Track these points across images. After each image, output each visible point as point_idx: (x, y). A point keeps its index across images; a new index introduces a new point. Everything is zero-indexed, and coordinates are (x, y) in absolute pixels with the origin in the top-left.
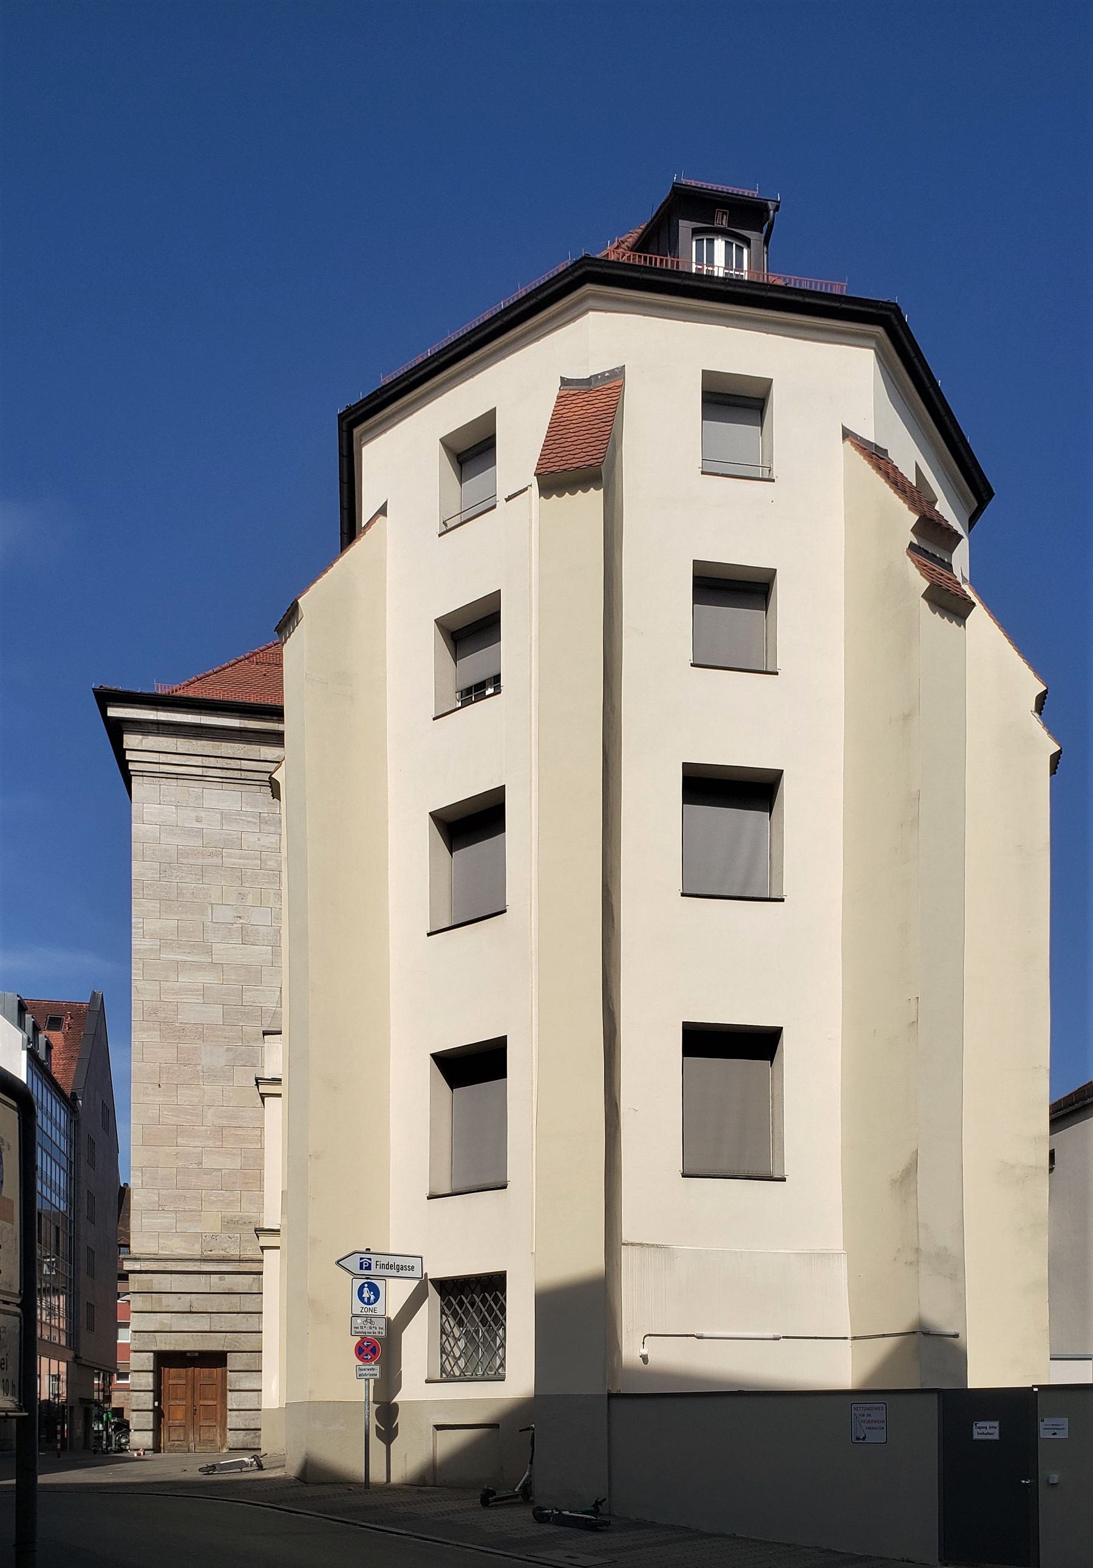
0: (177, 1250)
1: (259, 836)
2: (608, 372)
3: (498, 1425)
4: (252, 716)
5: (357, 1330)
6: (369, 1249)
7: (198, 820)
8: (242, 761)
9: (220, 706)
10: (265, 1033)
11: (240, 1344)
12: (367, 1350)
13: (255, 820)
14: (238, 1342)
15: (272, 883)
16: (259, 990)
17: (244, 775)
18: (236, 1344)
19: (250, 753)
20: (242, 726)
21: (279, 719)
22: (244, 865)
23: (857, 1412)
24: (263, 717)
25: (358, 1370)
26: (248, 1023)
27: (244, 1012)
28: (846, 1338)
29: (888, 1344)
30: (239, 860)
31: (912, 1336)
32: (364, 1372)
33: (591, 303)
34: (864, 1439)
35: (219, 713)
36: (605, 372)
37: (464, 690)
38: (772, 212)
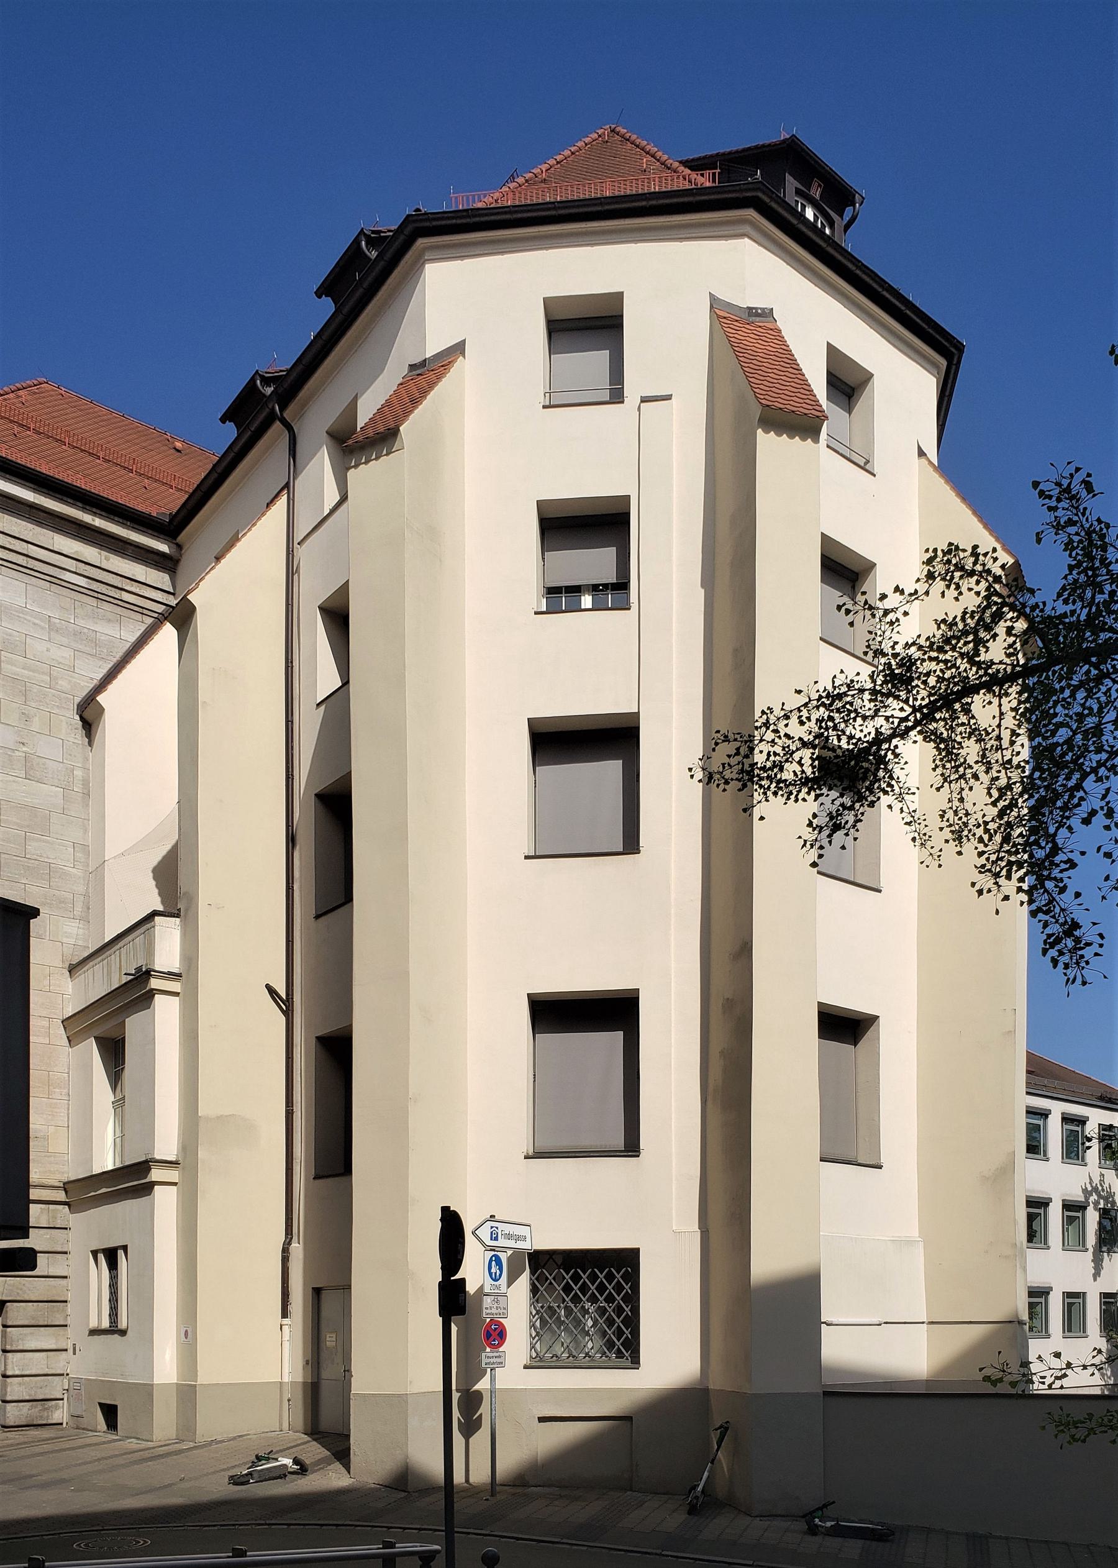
1: (49, 646)
2: (760, 308)
3: (632, 1417)
4: (51, 493)
6: (494, 1216)
8: (29, 545)
9: (13, 468)
11: (25, 1292)
12: (495, 1335)
13: (43, 624)
14: (21, 1289)
15: (64, 708)
16: (44, 841)
17: (32, 563)
18: (19, 1291)
19: (42, 538)
20: (36, 502)
21: (85, 506)
22: (28, 678)
24: (65, 498)
26: (32, 882)
27: (28, 867)
28: (923, 1323)
29: (975, 1333)
30: (23, 671)
31: (1010, 1325)
32: (492, 1360)
33: (747, 229)
35: (8, 476)
38: (857, 205)
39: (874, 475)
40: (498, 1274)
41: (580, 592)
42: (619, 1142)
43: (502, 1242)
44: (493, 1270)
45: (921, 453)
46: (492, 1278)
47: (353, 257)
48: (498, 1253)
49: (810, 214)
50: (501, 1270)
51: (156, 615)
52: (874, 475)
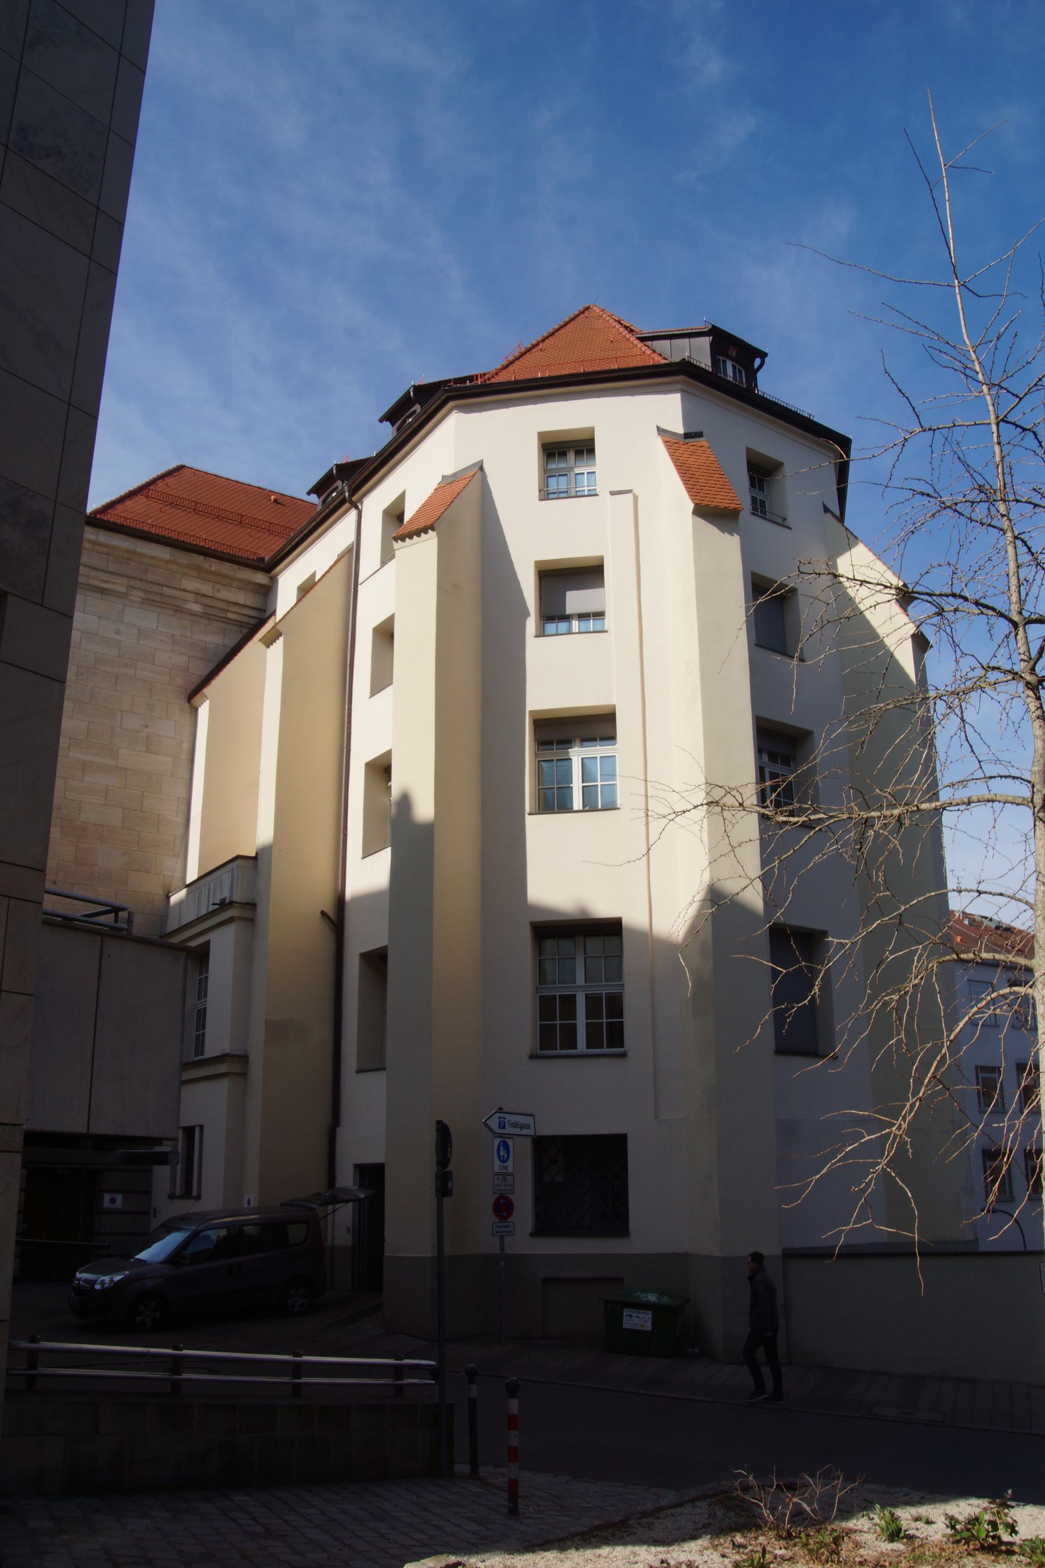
0: (940, 782)
5: (498, 1188)
7: (118, 632)
36: (692, 433)
37: (576, 614)
39: (790, 529)
43: (509, 1130)
44: (502, 1153)
45: (826, 510)
46: (500, 1160)
48: (506, 1140)
51: (251, 626)
52: (790, 529)
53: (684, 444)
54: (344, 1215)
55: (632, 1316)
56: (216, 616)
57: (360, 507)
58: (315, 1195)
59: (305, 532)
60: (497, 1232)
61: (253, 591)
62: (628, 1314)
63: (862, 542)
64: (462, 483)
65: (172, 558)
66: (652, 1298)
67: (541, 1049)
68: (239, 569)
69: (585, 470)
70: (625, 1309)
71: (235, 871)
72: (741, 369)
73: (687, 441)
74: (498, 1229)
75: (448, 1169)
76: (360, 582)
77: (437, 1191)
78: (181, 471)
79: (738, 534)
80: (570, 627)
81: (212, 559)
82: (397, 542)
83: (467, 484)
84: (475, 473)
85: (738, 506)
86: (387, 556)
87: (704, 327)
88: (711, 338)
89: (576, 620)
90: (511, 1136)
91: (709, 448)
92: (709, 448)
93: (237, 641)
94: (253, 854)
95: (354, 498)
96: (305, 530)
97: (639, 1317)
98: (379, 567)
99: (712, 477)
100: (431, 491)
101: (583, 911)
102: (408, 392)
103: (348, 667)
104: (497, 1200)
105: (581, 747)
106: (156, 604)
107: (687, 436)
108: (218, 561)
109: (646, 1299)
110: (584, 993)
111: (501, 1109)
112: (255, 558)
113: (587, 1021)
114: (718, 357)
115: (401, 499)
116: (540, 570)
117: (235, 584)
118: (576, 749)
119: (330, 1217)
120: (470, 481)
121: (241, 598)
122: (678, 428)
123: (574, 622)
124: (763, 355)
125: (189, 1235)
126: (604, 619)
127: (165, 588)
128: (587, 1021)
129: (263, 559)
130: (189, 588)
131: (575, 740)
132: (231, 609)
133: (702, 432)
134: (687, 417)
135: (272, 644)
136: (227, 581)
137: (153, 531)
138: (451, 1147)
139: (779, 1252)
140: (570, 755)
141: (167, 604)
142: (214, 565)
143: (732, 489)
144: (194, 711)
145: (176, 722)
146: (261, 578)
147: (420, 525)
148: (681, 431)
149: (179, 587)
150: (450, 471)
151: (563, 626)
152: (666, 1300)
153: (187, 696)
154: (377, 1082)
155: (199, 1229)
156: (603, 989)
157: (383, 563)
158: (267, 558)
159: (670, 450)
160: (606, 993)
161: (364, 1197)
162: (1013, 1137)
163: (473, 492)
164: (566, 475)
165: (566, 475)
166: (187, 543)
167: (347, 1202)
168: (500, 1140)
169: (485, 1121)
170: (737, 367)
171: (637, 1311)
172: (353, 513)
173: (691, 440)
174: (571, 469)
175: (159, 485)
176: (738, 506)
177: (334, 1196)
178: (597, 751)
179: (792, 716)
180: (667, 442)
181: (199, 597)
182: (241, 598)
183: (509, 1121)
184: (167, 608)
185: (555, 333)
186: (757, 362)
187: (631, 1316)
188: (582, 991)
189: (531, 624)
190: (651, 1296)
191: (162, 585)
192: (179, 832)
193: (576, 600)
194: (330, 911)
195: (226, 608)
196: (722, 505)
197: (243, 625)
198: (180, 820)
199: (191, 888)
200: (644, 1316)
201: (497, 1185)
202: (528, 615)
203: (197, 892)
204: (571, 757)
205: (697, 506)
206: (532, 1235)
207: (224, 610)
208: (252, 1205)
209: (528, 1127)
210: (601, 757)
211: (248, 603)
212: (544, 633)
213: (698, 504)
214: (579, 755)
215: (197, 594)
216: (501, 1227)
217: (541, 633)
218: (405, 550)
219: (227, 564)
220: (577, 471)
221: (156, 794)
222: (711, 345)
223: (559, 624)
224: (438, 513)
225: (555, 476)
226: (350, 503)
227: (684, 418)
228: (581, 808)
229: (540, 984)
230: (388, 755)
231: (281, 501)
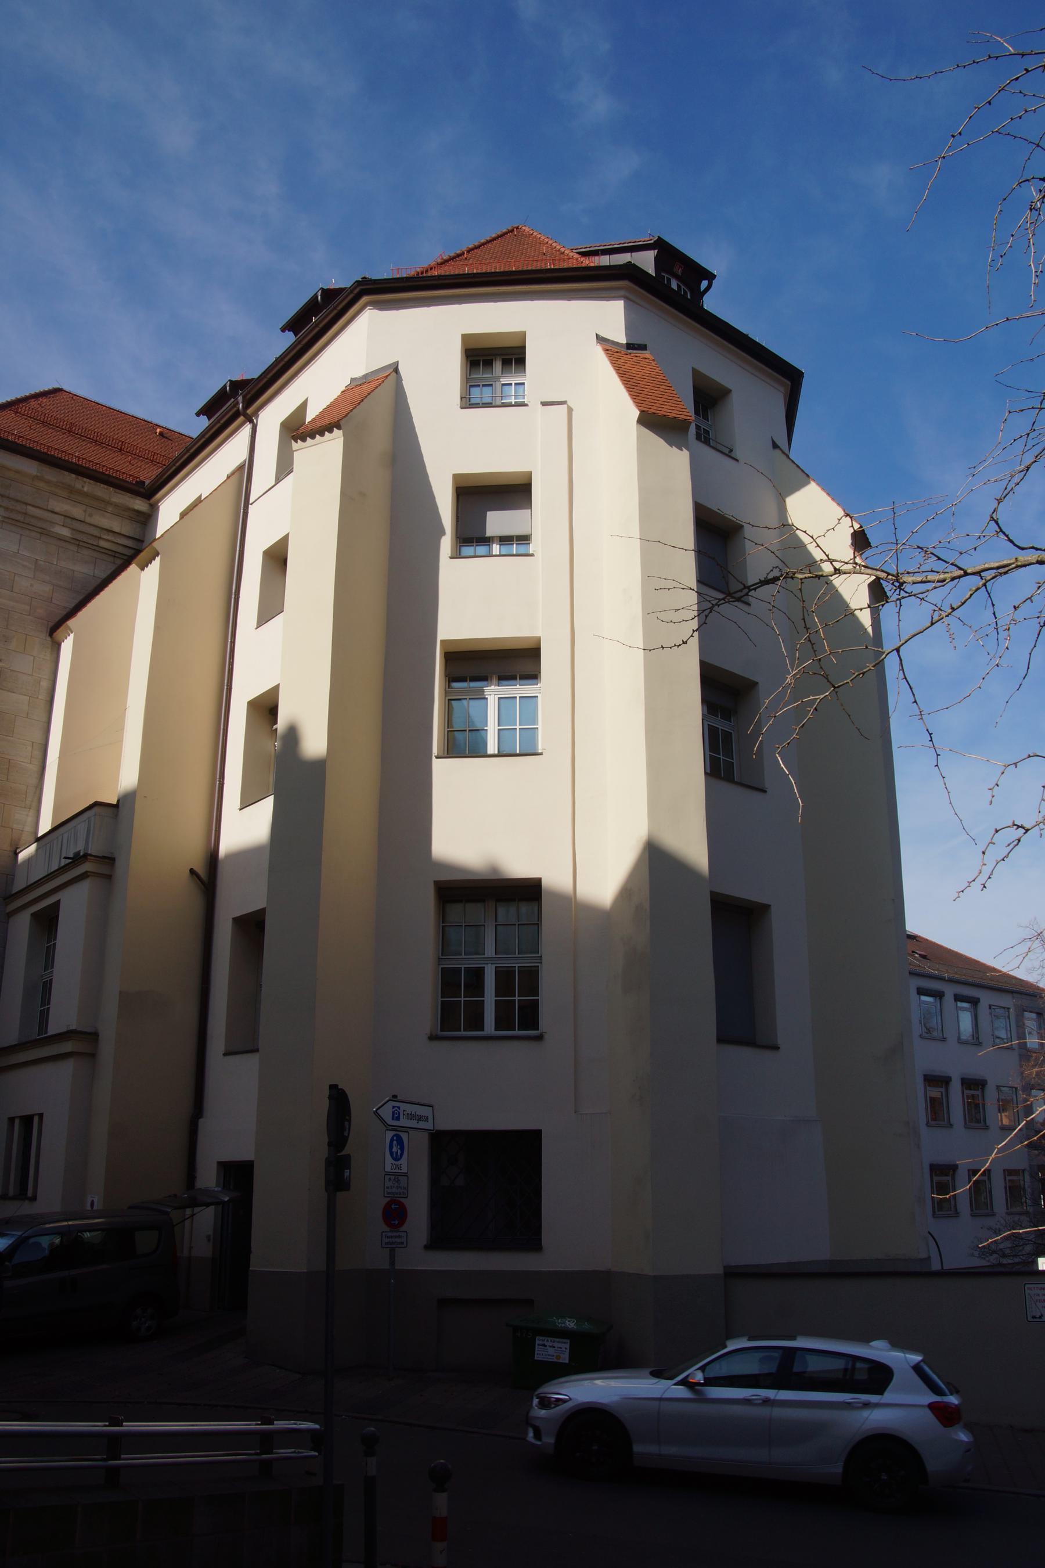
2: (637, 344)
5: (390, 1191)
10: (994, 958)
23: (1029, 1291)
25: (384, 1236)
34: (1040, 1317)
36: (635, 344)
39: (737, 460)
40: (399, 1154)
41: (489, 542)
42: (536, 926)
43: (404, 1122)
44: (394, 1150)
47: (311, 308)
48: (400, 1133)
49: (674, 285)
50: (402, 1149)
51: (125, 558)
52: (737, 460)
53: (627, 354)
54: (206, 1219)
55: (545, 1346)
56: (87, 543)
57: (255, 420)
58: (170, 1196)
59: (192, 451)
60: (386, 1243)
61: (131, 519)
62: (541, 1343)
63: (814, 480)
64: (376, 383)
65: (39, 474)
66: (570, 1324)
67: (442, 1030)
68: (115, 492)
69: (513, 380)
70: (537, 1338)
71: (93, 818)
72: (687, 290)
73: (629, 351)
74: (387, 1240)
75: (343, 1153)
76: (251, 501)
77: (328, 1183)
78: (58, 394)
79: (688, 449)
80: (490, 550)
81: (85, 479)
82: (297, 442)
83: (380, 384)
84: (389, 375)
85: (689, 418)
86: (284, 467)
87: (649, 239)
88: (656, 251)
89: (497, 544)
90: (406, 1129)
91: (653, 360)
92: (653, 360)
93: (109, 572)
94: (115, 802)
95: (249, 411)
96: (191, 448)
97: (554, 1347)
98: (273, 483)
99: (659, 388)
100: (339, 393)
101: (495, 870)
102: (315, 296)
103: (233, 596)
104: (388, 1205)
105: (498, 686)
106: (19, 524)
107: (630, 346)
108: (92, 482)
109: (563, 1325)
110: (493, 966)
111: (395, 1096)
112: (134, 482)
113: (497, 998)
114: (663, 274)
115: (303, 407)
116: (459, 486)
117: (110, 509)
118: (493, 687)
119: (187, 1223)
120: (383, 381)
121: (116, 525)
122: (620, 337)
123: (494, 545)
124: (710, 277)
125: (13, 1243)
126: (529, 543)
127: (29, 507)
128: (497, 998)
129: (144, 482)
130: (57, 509)
131: (491, 677)
132: (105, 537)
133: (646, 345)
134: (629, 327)
135: (147, 566)
136: (101, 505)
137: (20, 441)
138: (349, 1121)
139: (720, 1271)
140: (485, 694)
141: (30, 525)
142: (87, 486)
143: (680, 401)
144: (57, 647)
145: (34, 657)
146: (139, 505)
147: (327, 421)
148: (622, 340)
149: (45, 508)
150: (360, 372)
151: (481, 550)
152: (586, 1326)
153: (49, 630)
154: (248, 1066)
155: (26, 1235)
156: (517, 961)
157: (278, 480)
158: (147, 482)
159: (611, 358)
160: (518, 967)
161: (228, 1201)
162: (1035, 1136)
163: (384, 395)
164: (491, 385)
165: (491, 385)
166: (57, 458)
167: (208, 1205)
168: (392, 1133)
169: (377, 1110)
170: (682, 287)
171: (553, 1339)
172: (247, 429)
173: (635, 351)
174: (498, 379)
175: (31, 403)
176: (689, 418)
177: (194, 1200)
178: (518, 690)
179: (733, 664)
180: (608, 350)
181: (69, 521)
182: (116, 525)
183: (404, 1111)
184: (30, 530)
185: (481, 246)
186: (704, 284)
187: (544, 1345)
188: (492, 964)
189: (446, 544)
190: (569, 1321)
191: (26, 504)
192: (34, 781)
193: (497, 522)
194: (201, 870)
195: (98, 535)
196: (671, 415)
197: (117, 555)
198: (34, 768)
199: (42, 842)
200: (560, 1345)
201: (388, 1188)
202: (443, 533)
203: (48, 845)
204: (486, 696)
205: (643, 413)
206: (427, 1247)
207: (96, 537)
208: (95, 1208)
209: (426, 1119)
210: (520, 697)
211: (124, 532)
212: (460, 554)
213: (644, 411)
214: (495, 695)
215: (65, 516)
216: (392, 1237)
217: (456, 555)
218: (305, 453)
219: (102, 485)
220: (504, 381)
221: (7, 736)
222: (656, 258)
223: (478, 548)
224: (345, 411)
225: (479, 386)
226: (244, 416)
227: (627, 328)
228: (496, 752)
229: (442, 955)
230: (274, 692)
231: (166, 435)
